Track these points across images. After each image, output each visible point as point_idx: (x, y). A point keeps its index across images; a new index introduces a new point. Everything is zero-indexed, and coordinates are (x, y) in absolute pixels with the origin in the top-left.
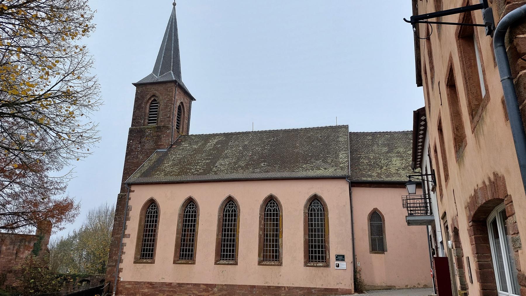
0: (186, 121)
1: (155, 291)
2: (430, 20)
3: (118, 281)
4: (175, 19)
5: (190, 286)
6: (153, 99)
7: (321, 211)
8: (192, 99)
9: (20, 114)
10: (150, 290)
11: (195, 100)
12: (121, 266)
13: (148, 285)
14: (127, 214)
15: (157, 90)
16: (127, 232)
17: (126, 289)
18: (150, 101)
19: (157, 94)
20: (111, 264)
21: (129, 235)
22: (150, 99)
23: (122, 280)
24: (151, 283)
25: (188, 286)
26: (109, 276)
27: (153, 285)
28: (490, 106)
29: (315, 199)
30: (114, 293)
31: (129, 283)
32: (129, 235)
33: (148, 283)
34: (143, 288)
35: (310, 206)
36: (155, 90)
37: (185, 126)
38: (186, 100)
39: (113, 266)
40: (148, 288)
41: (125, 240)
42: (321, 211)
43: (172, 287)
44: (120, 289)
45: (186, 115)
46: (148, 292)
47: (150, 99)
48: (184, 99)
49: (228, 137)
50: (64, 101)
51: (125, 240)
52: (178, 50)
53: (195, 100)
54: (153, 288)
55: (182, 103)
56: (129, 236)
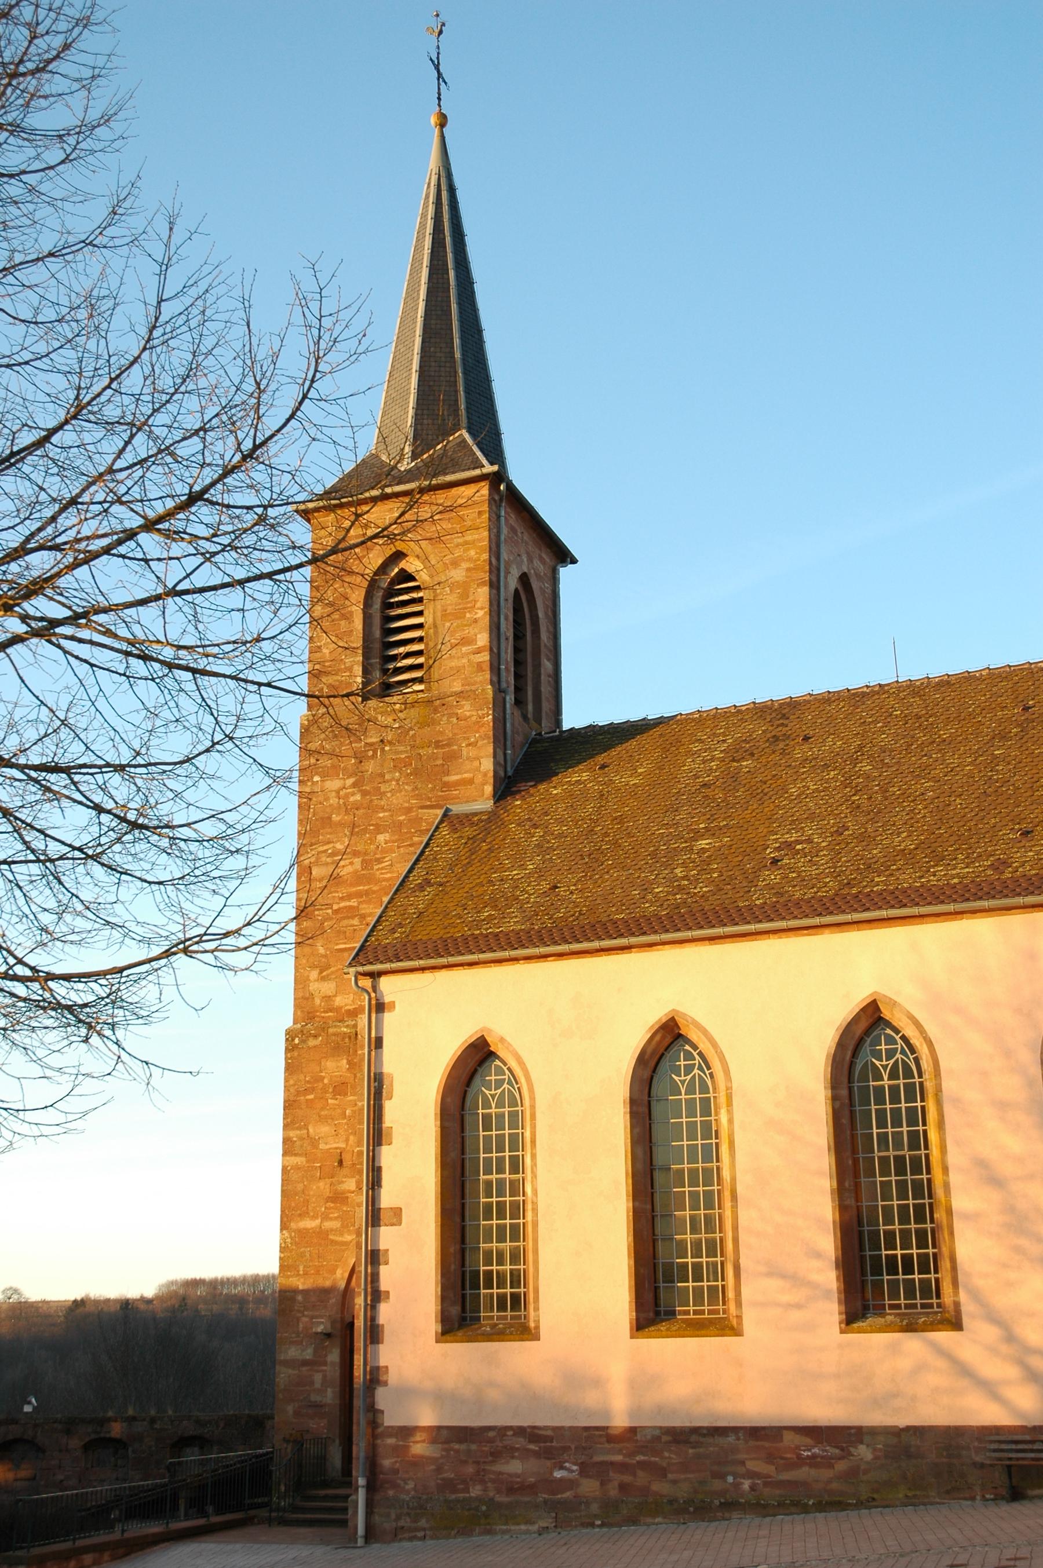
0: (547, 665)
2: (170, 504)
4: (452, 190)
5: (731, 1439)
7: (908, 1073)
8: (563, 556)
9: (245, 551)
11: (574, 561)
25: (721, 1440)
27: (551, 1439)
28: (942, 1230)
30: (362, 1481)
37: (546, 689)
38: (537, 563)
40: (526, 1454)
43: (642, 1449)
45: (544, 636)
48: (530, 560)
49: (781, 723)
52: (479, 331)
53: (574, 561)
55: (524, 579)
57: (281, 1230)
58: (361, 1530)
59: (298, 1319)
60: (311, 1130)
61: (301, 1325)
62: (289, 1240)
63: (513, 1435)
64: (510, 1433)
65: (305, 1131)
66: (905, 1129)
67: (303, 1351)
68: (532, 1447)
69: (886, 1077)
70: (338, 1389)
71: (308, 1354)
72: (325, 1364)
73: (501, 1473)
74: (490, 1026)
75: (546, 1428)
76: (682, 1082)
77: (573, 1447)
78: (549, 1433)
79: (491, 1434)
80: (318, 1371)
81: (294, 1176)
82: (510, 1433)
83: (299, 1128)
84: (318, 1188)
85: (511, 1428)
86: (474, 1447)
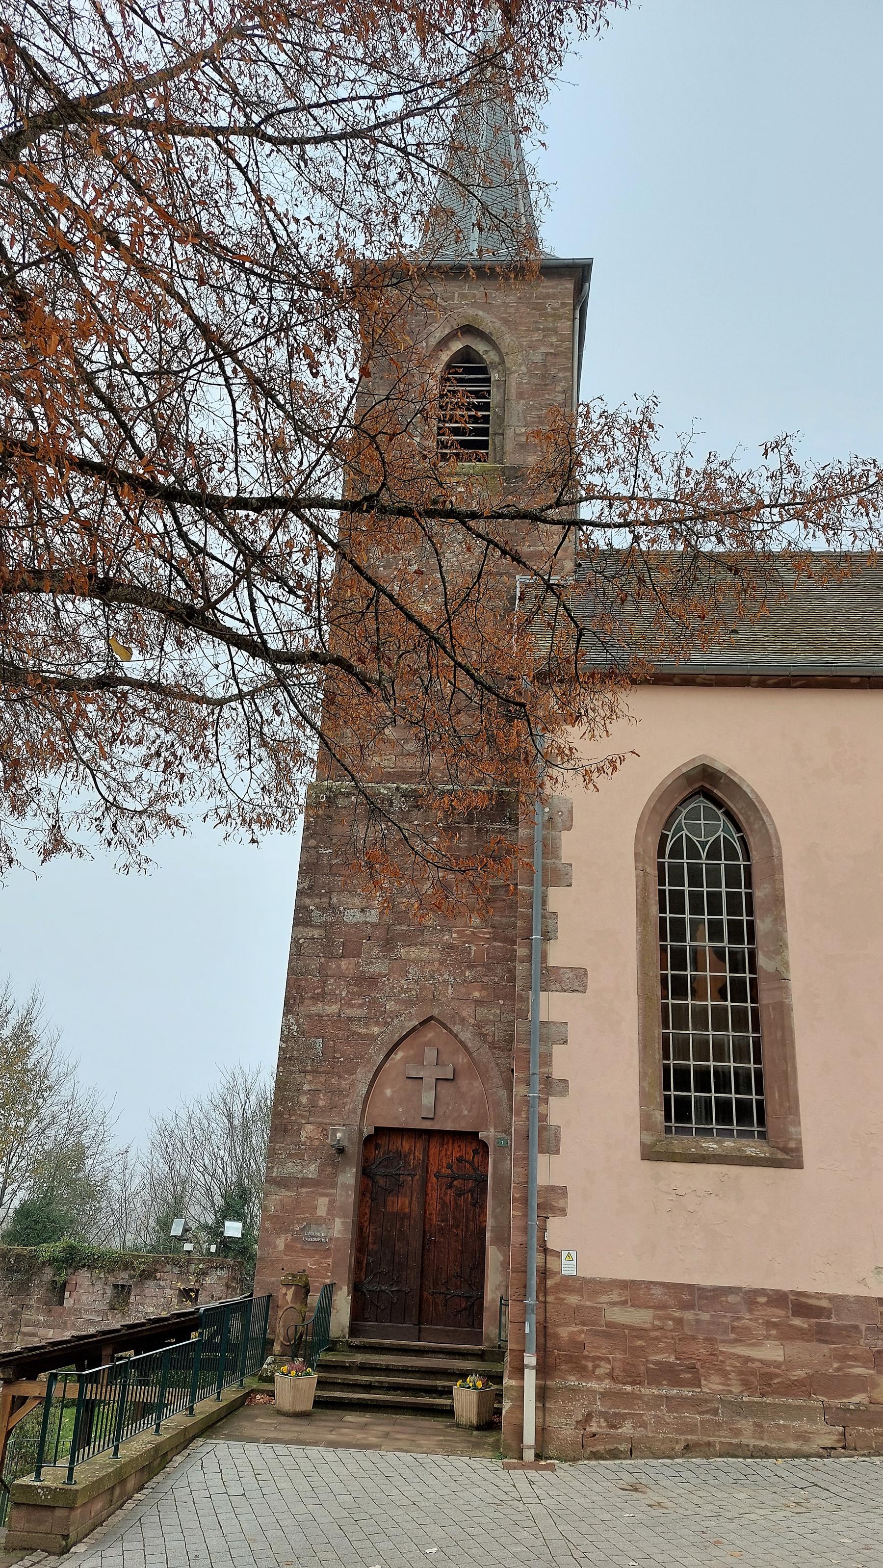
1: (844, 1357)
3: (544, 1273)
6: (457, 346)
7: (731, 854)
10: (798, 1350)
12: (548, 1171)
13: (777, 1314)
14: (550, 849)
15: (487, 306)
16: (559, 955)
17: (613, 1333)
18: (445, 357)
19: (488, 321)
20: (291, 1168)
21: (581, 974)
22: (444, 343)
23: (568, 1268)
24: (800, 1305)
26: (280, 1243)
27: (819, 1312)
29: (705, 786)
31: (633, 1291)
32: (581, 974)
33: (778, 1298)
34: (743, 1336)
35: (667, 825)
36: (474, 305)
39: (305, 1182)
40: (787, 1334)
41: (552, 1006)
42: (731, 854)
44: (564, 1332)
46: (789, 1364)
47: (444, 343)
50: (357, 358)
51: (552, 1006)
54: (822, 1334)
56: (577, 980)
57: (285, 1015)
58: (529, 1437)
59: (301, 1127)
60: (334, 900)
61: (303, 1134)
62: (295, 1027)
63: (767, 1303)
64: (762, 1300)
65: (327, 900)
66: (725, 917)
67: (303, 1167)
68: (797, 1322)
69: (704, 856)
70: (350, 1220)
71: (312, 1171)
72: (334, 1185)
73: (748, 1359)
74: (713, 754)
75: (819, 1296)
76: (703, 845)
77: (863, 1327)
78: (824, 1303)
79: (731, 1299)
80: (326, 1195)
81: (307, 950)
82: (762, 1300)
83: (320, 896)
84: (339, 967)
85: (763, 1292)
86: (705, 1317)
